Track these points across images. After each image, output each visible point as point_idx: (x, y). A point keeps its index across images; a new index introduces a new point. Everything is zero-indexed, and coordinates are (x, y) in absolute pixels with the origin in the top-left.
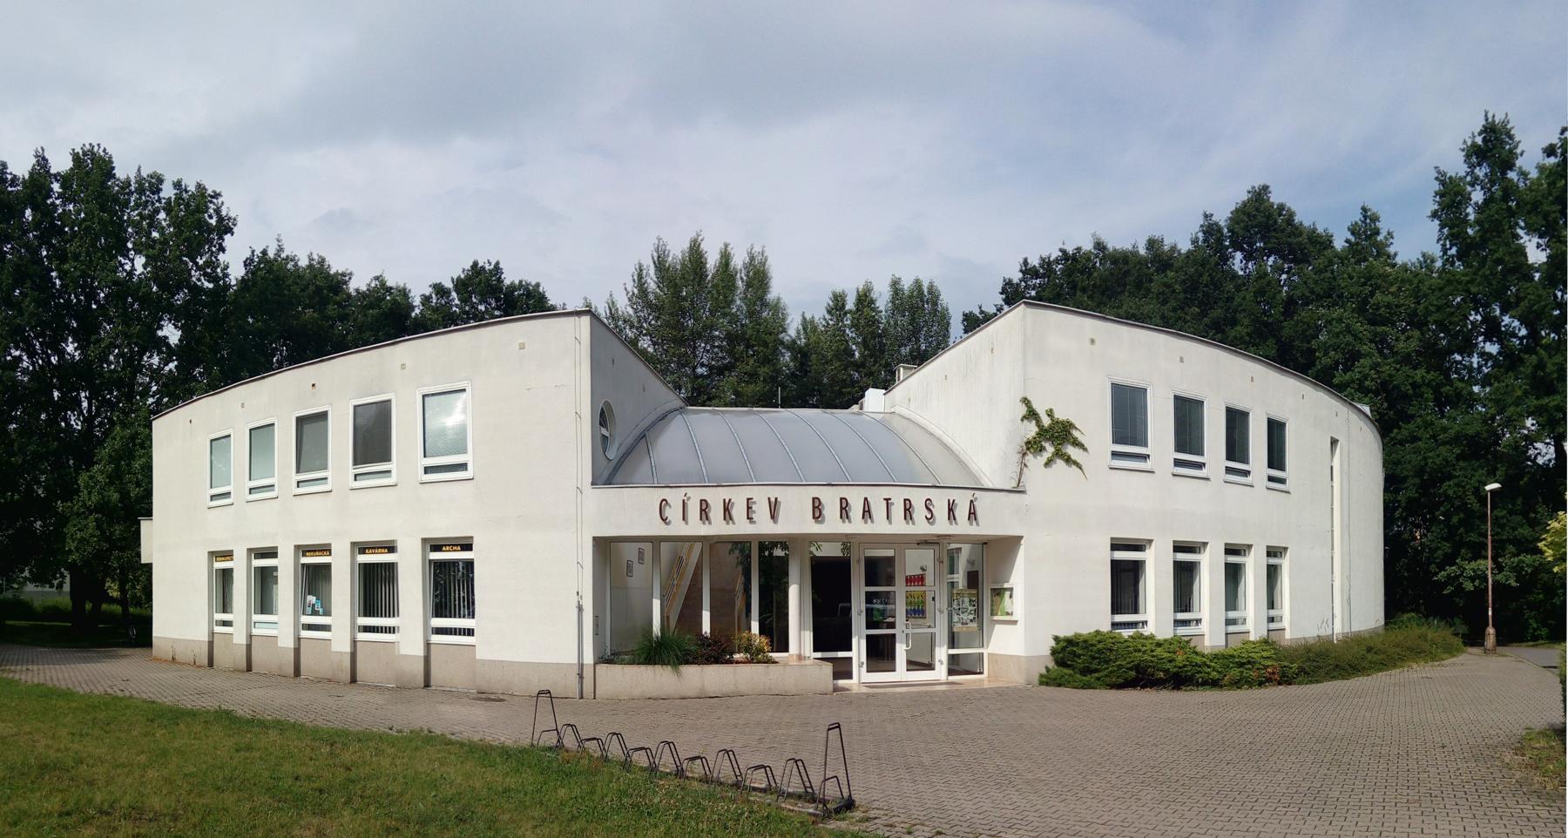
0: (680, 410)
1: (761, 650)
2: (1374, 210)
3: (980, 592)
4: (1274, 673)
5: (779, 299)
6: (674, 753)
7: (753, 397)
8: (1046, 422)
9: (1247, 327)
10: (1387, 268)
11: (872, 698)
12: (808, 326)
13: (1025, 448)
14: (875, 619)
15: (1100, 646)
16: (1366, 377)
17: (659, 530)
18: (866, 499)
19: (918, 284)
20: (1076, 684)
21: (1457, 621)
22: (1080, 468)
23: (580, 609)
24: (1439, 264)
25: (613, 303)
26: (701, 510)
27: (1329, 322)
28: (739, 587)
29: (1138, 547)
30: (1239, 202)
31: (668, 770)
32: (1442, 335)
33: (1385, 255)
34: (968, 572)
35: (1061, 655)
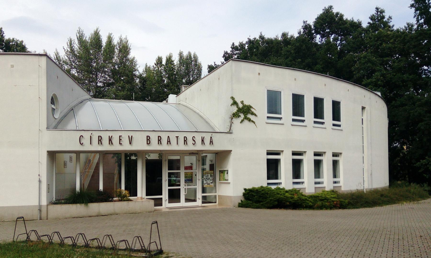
0: (89, 100)
1: (125, 196)
2: (382, 8)
3: (215, 172)
4: (337, 204)
5: (134, 58)
6: (84, 238)
7: (123, 96)
8: (241, 106)
9: (321, 65)
10: (389, 32)
11: (171, 213)
12: (147, 69)
13: (232, 116)
14: (172, 183)
15: (263, 192)
16: (378, 80)
17: (78, 148)
18: (168, 137)
19: (190, 54)
20: (253, 207)
21: (425, 185)
22: (254, 123)
23: (40, 181)
24: (415, 27)
25: (58, 53)
26: (99, 140)
27: (360, 59)
28: (116, 172)
29: (278, 154)
30: (319, 14)
31: (81, 245)
32: (417, 58)
33: (387, 27)
34: (210, 165)
35: (247, 196)
